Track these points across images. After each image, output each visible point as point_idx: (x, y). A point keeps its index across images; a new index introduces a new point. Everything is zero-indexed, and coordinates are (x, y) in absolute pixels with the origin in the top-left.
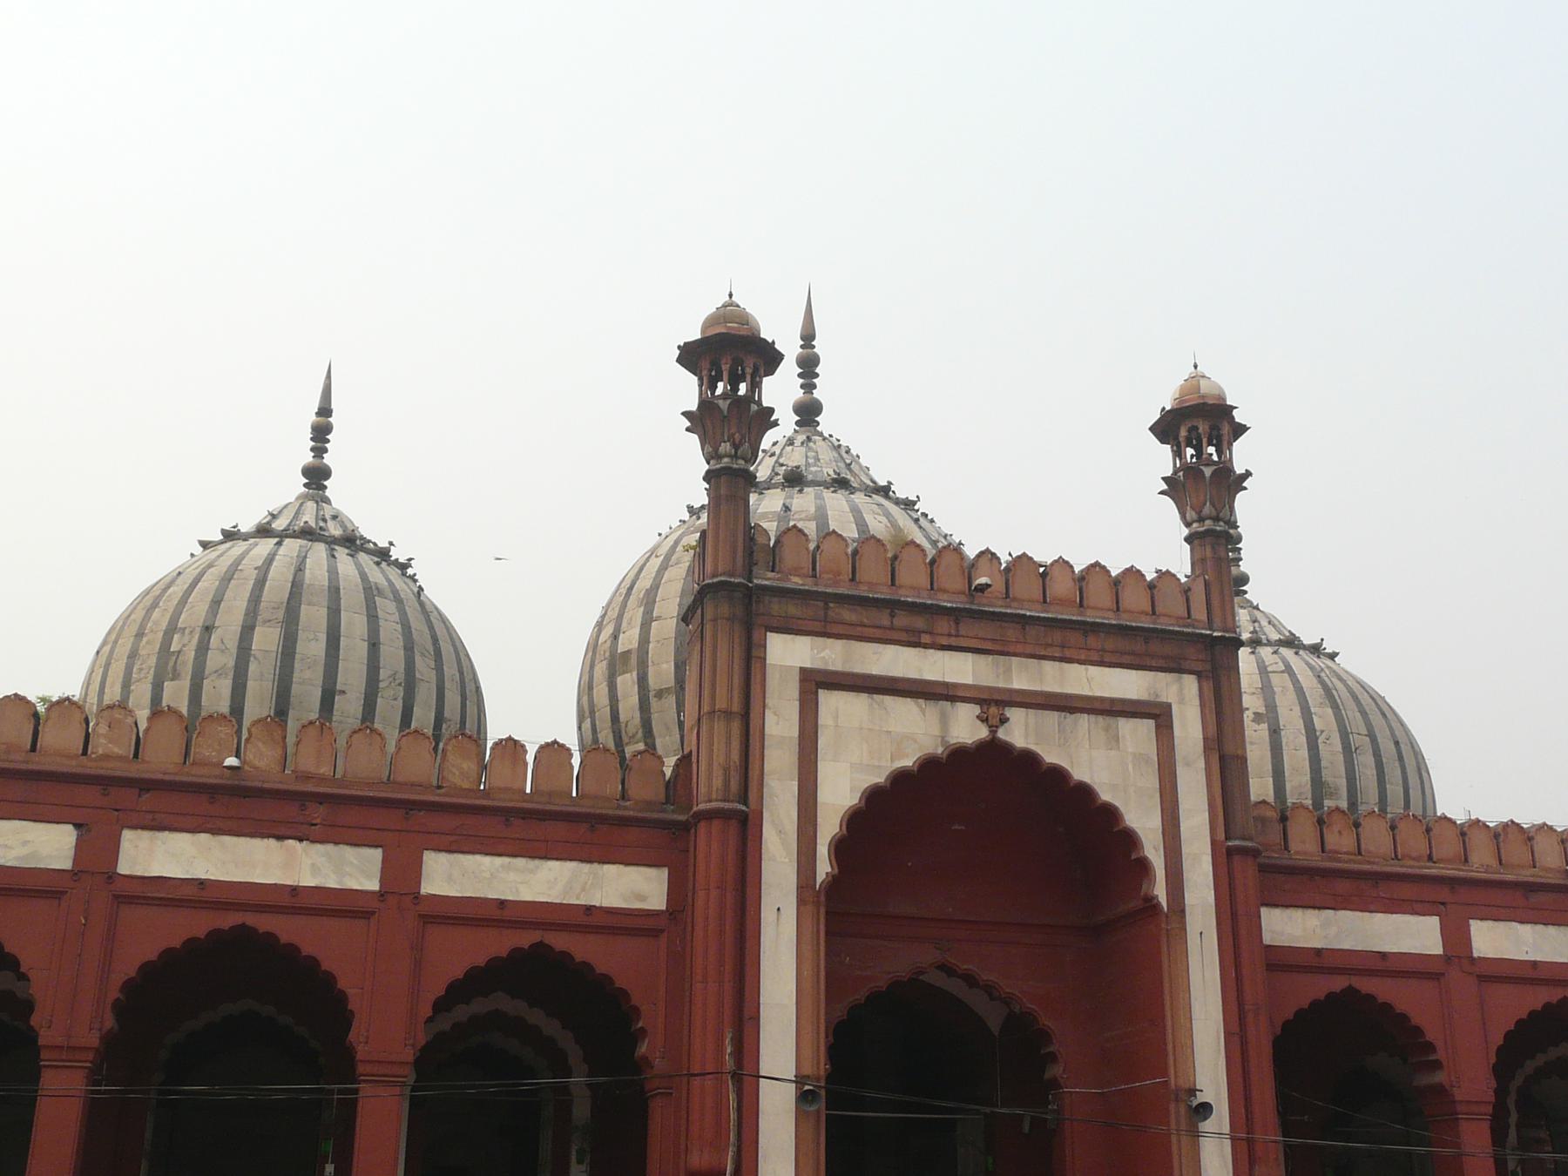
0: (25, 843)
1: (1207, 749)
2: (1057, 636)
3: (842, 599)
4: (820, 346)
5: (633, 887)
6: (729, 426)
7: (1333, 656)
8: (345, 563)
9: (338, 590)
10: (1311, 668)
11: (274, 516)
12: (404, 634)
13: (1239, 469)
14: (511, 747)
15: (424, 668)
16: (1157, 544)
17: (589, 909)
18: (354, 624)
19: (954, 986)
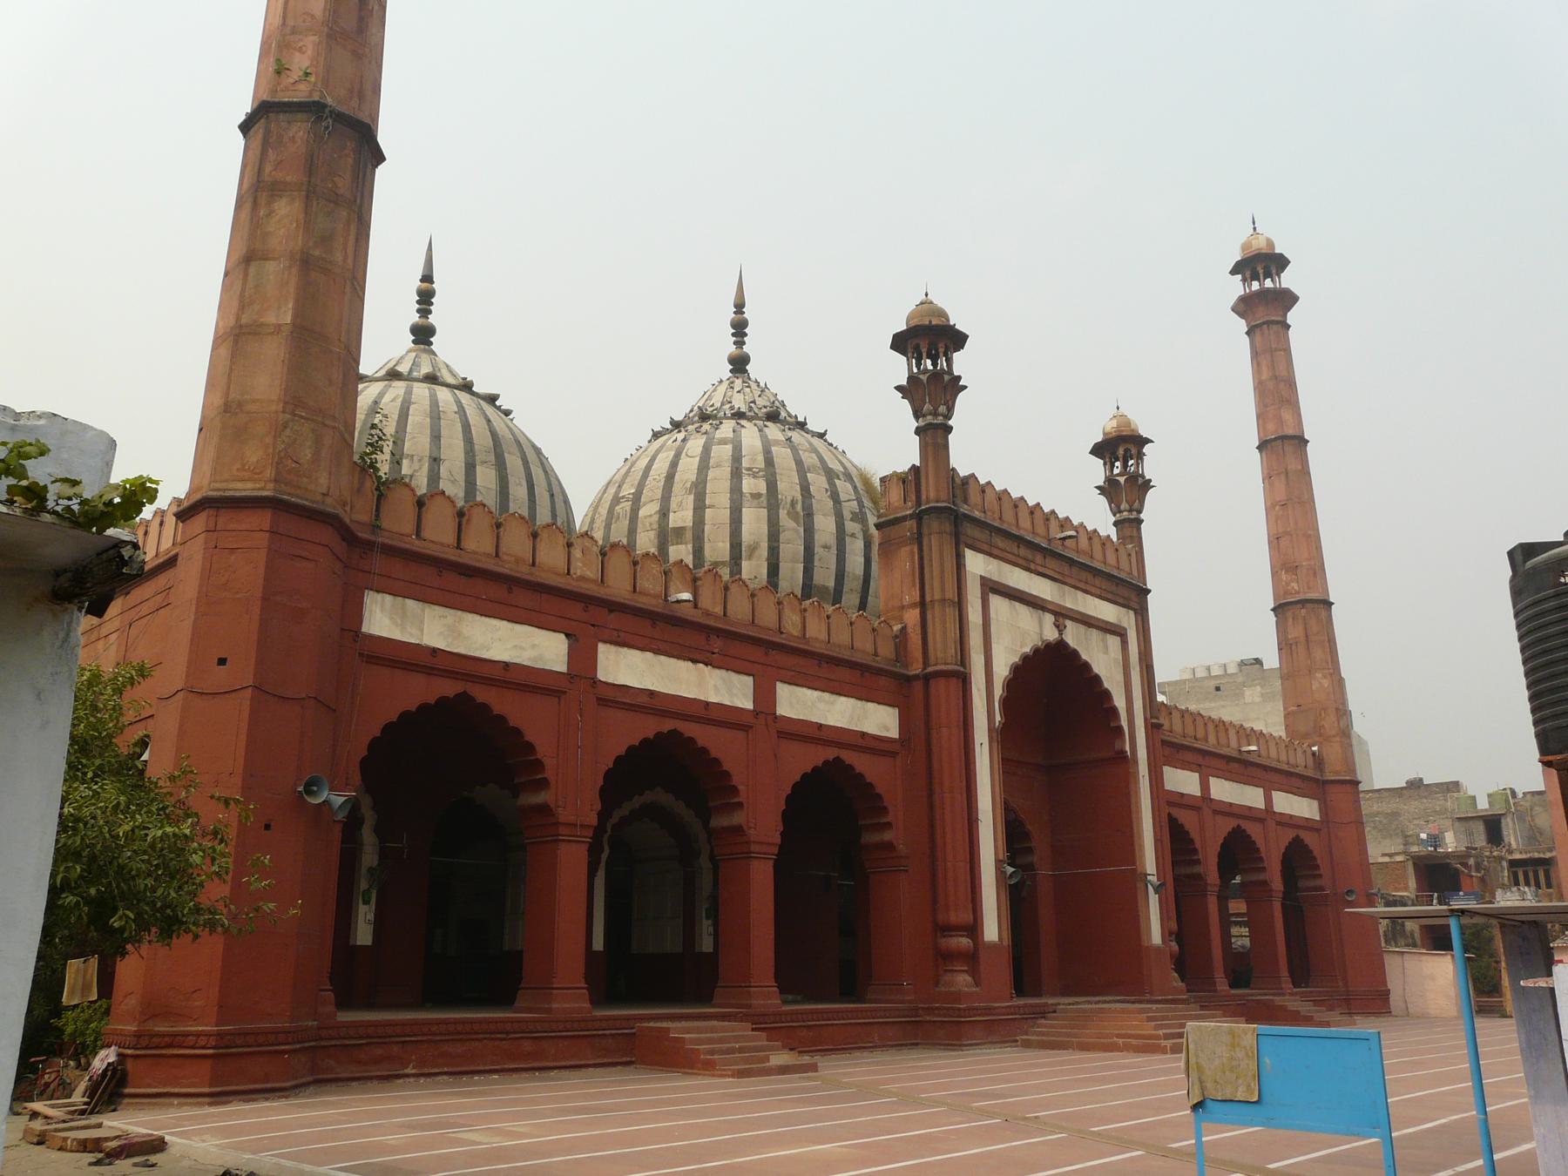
0: (534, 646)
4: (748, 313)
5: (880, 720)
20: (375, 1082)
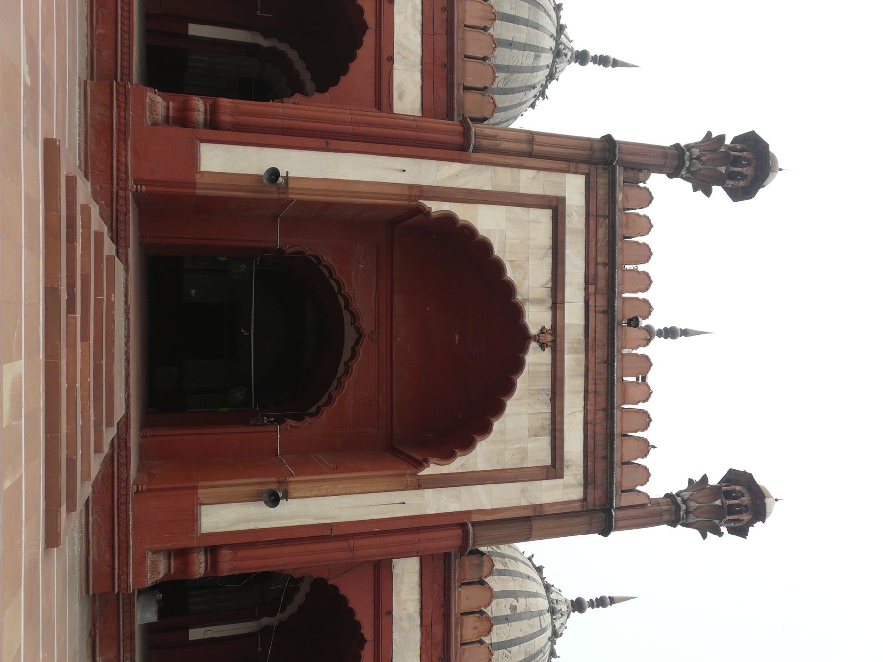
1: (535, 507)
2: (601, 388)
4: (682, 339)
8: (542, 75)
9: (537, 29)
12: (516, 67)
17: (391, 59)
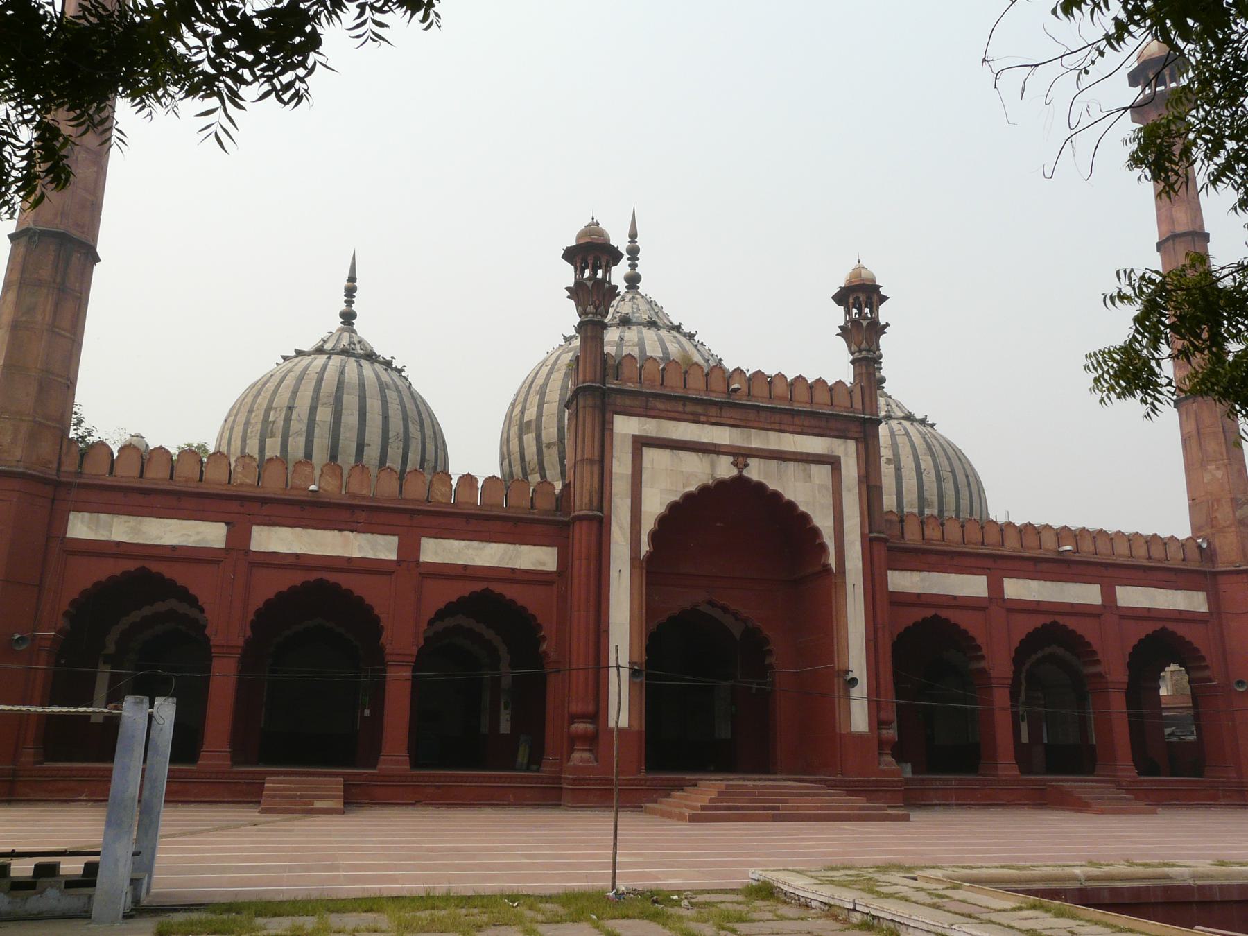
0: (198, 533)
1: (860, 482)
2: (777, 418)
3: (656, 396)
4: (640, 241)
5: (537, 558)
6: (592, 296)
7: (932, 426)
9: (364, 385)
10: (920, 433)
11: (325, 342)
13: (882, 322)
14: (468, 480)
15: (414, 430)
16: (836, 365)
17: (514, 570)
18: (374, 405)
19: (717, 613)
20: (941, 808)
